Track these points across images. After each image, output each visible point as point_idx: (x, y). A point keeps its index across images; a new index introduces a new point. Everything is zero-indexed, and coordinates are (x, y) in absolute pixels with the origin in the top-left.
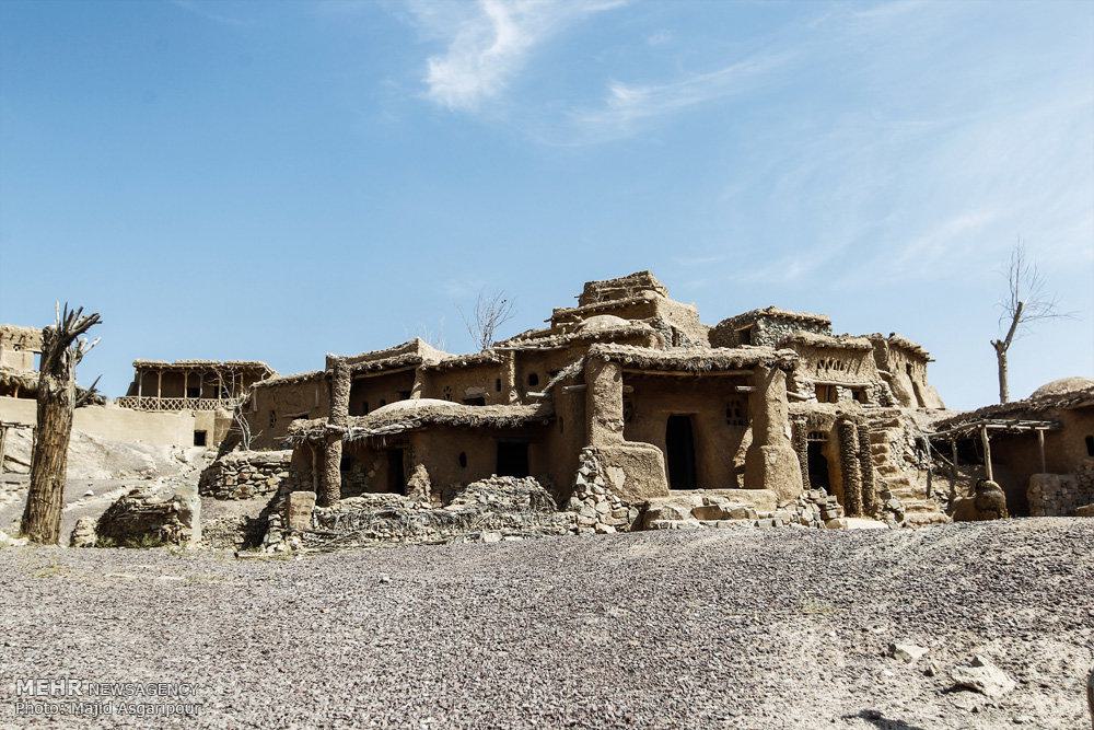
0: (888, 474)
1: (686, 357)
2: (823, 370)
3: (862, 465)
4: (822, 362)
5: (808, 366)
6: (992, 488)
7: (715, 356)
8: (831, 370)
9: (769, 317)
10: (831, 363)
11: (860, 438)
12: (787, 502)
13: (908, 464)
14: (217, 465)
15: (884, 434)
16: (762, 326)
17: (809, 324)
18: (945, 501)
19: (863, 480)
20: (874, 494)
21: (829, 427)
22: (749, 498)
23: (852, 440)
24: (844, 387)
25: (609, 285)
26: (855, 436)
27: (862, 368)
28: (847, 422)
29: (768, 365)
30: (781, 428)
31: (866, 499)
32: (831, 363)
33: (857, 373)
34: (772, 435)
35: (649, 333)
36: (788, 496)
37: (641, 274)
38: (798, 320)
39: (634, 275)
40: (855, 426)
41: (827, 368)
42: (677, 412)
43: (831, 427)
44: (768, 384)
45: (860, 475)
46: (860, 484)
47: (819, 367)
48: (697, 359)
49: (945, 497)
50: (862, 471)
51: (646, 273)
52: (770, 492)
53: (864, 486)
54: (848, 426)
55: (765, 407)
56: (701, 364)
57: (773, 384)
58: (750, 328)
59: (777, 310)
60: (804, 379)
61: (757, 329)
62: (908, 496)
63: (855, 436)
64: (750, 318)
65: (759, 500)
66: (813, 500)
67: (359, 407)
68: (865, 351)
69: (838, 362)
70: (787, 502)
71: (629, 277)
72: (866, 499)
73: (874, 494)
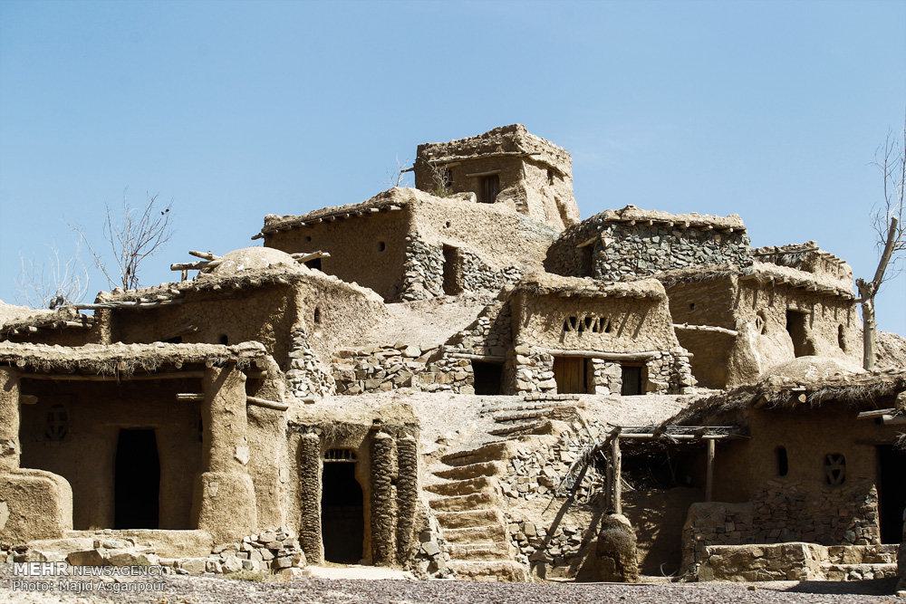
0: (480, 506)
1: (102, 357)
2: (574, 333)
3: (399, 494)
4: (573, 320)
5: (548, 327)
6: (619, 524)
7: (145, 355)
8: (588, 333)
9: (624, 226)
10: (588, 321)
11: (399, 457)
12: (225, 546)
13: (542, 489)
14: (493, 452)
15: (503, 446)
16: (608, 241)
17: (701, 232)
18: (576, 542)
19: (398, 515)
20: (411, 535)
21: (356, 443)
22: (169, 541)
23: (386, 459)
24: (607, 360)
25: (452, 150)
26: (393, 456)
27: (645, 327)
28: (381, 435)
29: (216, 365)
30: (230, 449)
31: (401, 542)
32: (588, 321)
33: (635, 336)
34: (216, 458)
35: (295, 279)
36: (227, 538)
37: (505, 130)
38: (679, 226)
39: (494, 132)
40: (394, 440)
41: (581, 330)
42: (126, 425)
43: (360, 442)
44: (217, 390)
45: (394, 508)
46: (394, 521)
47: (566, 329)
48: (118, 359)
49: (577, 538)
50: (399, 503)
51: (513, 129)
52: (202, 534)
53: (400, 523)
54: (380, 441)
55: (210, 422)
56: (124, 366)
57: (223, 390)
58: (594, 242)
59: (638, 213)
60: (536, 349)
61: (601, 245)
62: (482, 537)
63: (393, 456)
64: (592, 228)
65: (184, 543)
66: (265, 543)
67: (214, 365)
68: (651, 300)
69: (602, 321)
70: (225, 546)
71: (486, 136)
72: (401, 542)
73: (411, 535)
